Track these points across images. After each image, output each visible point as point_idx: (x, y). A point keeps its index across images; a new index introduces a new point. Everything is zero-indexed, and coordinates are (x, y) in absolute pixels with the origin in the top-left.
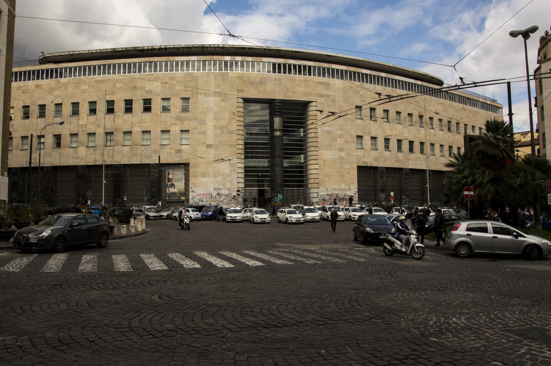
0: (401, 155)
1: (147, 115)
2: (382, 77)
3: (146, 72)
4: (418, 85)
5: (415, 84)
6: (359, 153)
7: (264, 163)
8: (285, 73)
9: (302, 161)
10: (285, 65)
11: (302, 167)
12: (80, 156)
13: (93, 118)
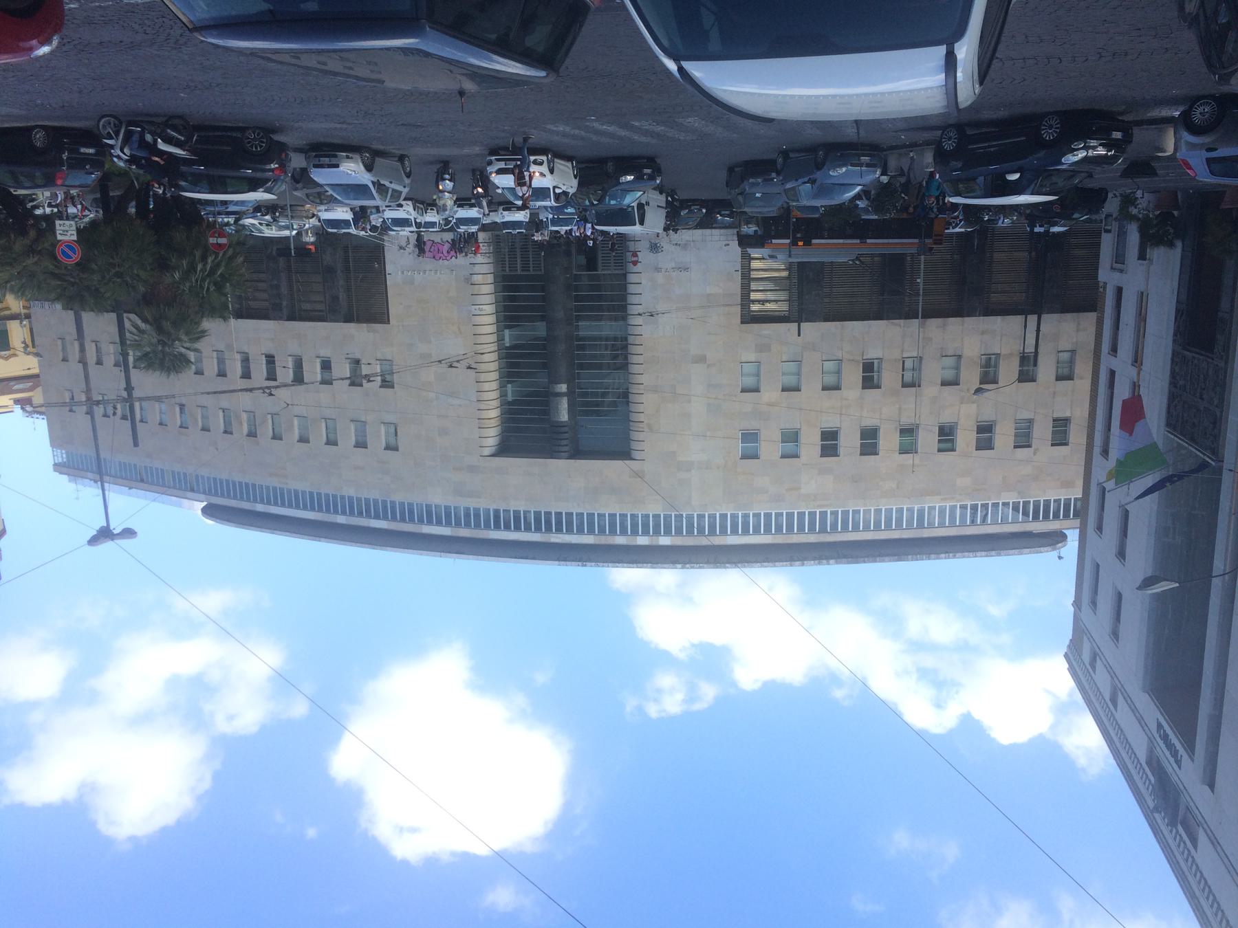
0: (294, 348)
1: (830, 422)
2: (344, 513)
3: (832, 513)
4: (262, 502)
5: (269, 503)
6: (387, 352)
7: (587, 328)
8: (548, 514)
9: (507, 332)
10: (549, 529)
11: (511, 319)
12: (971, 337)
13: (947, 418)
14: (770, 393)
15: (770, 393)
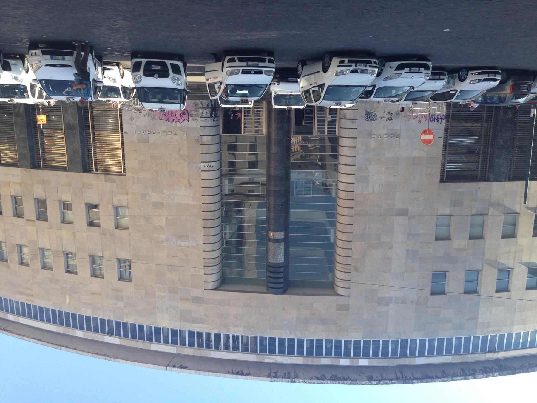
0: (39, 193)
2: (82, 328)
10: (263, 351)
14: (459, 241)
15: (459, 241)
